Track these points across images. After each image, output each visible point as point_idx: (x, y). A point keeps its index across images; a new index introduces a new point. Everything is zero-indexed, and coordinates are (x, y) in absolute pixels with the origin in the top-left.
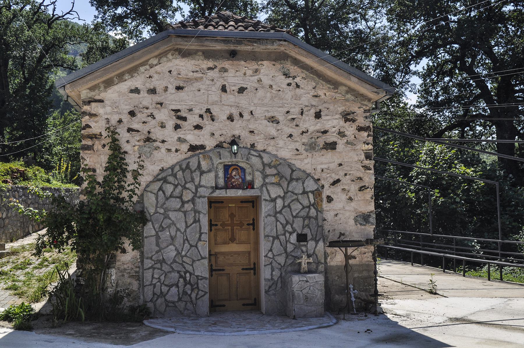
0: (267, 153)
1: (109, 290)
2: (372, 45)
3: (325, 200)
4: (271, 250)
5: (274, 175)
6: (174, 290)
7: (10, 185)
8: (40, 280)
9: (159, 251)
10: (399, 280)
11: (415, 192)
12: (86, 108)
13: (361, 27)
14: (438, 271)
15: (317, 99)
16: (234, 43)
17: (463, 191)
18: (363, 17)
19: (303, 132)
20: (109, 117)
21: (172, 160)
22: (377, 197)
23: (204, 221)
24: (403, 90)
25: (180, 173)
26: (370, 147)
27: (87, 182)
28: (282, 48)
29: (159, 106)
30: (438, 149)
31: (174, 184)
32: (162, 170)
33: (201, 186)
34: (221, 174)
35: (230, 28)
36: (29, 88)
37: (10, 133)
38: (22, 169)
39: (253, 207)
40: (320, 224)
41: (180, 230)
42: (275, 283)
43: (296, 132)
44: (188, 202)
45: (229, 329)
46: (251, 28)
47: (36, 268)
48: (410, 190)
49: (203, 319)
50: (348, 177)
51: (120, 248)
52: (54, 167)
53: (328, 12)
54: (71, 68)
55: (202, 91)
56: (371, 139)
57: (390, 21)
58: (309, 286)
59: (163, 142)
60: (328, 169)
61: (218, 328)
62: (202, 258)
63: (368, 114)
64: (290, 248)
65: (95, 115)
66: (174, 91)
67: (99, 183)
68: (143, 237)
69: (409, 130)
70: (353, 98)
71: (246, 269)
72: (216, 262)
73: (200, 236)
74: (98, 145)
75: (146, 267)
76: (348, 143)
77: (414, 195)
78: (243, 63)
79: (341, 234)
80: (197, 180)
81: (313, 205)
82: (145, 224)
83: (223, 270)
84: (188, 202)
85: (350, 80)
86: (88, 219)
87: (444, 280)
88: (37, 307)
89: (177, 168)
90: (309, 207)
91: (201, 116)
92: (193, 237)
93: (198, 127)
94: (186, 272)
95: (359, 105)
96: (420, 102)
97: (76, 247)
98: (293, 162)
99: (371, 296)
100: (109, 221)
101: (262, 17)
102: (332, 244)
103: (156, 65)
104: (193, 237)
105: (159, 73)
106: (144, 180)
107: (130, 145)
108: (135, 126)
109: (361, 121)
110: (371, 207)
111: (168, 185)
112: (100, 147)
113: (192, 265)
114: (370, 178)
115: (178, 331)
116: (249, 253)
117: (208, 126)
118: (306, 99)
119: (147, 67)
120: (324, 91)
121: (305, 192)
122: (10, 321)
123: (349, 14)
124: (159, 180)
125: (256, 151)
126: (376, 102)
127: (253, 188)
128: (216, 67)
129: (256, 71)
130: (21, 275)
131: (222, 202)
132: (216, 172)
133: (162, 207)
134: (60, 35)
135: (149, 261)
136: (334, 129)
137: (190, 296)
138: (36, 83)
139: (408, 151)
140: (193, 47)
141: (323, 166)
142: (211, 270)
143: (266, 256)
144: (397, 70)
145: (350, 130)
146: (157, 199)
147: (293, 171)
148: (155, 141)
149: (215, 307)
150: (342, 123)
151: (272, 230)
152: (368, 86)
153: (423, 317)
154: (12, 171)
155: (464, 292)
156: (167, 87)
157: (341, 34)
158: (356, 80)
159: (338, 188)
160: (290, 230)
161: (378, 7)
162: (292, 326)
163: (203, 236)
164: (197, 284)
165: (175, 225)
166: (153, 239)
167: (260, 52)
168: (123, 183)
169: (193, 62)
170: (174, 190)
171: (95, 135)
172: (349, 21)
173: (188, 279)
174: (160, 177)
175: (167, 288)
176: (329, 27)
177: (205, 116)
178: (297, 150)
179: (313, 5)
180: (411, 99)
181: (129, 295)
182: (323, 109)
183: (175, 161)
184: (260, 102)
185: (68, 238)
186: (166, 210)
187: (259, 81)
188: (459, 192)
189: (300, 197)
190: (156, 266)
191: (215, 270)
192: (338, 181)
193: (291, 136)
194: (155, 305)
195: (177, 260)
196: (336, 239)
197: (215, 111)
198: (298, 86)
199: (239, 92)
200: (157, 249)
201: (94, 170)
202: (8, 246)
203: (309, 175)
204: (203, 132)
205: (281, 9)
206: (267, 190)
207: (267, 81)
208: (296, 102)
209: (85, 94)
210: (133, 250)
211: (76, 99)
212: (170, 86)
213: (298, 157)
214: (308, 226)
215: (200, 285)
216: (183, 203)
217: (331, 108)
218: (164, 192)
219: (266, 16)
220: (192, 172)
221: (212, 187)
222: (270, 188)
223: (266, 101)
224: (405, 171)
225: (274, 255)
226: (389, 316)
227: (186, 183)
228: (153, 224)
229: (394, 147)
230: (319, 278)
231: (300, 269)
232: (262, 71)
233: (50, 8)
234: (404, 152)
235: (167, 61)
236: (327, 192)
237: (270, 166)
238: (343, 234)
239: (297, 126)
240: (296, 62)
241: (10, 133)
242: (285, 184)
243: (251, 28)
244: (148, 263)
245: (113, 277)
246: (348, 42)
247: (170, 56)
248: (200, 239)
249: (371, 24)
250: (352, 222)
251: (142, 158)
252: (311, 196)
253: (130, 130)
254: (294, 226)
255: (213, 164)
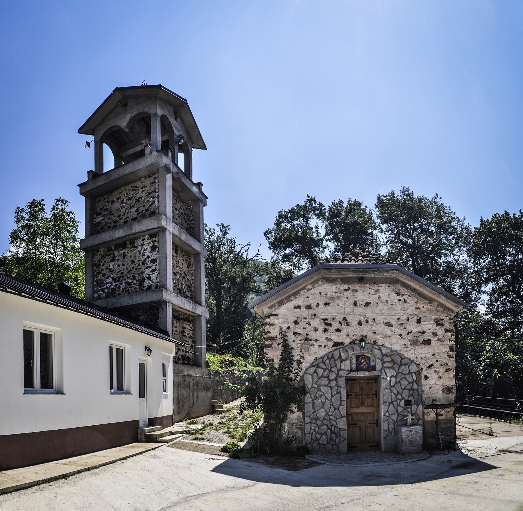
0: (385, 347)
1: (284, 436)
2: (457, 272)
3: (423, 378)
4: (388, 411)
5: (389, 362)
6: (324, 437)
7: (224, 370)
8: (243, 428)
9: (315, 412)
10: (471, 427)
11: (483, 370)
12: (267, 320)
13: (450, 260)
14: (495, 420)
15: (418, 310)
16: (362, 272)
17: (512, 370)
18: (452, 252)
19: (409, 333)
20: (281, 325)
21: (322, 352)
22: (457, 374)
23: (344, 392)
24: (477, 303)
25: (328, 361)
26: (453, 343)
27: (269, 368)
28: (395, 275)
29: (313, 317)
30: (497, 344)
31: (323, 369)
32: (316, 359)
33: (341, 370)
34: (354, 361)
35: (359, 261)
36: (233, 307)
37: (223, 336)
38: (230, 359)
39: (376, 383)
40: (420, 394)
41: (328, 399)
42: (391, 432)
43: (404, 333)
44: (333, 380)
45: (360, 462)
46: (373, 261)
47: (240, 420)
48: (480, 369)
49: (344, 456)
50: (438, 362)
51: (290, 410)
52: (250, 356)
53: (428, 248)
54: (258, 292)
55: (340, 306)
56: (453, 337)
57: (469, 256)
58: (411, 433)
59: (316, 340)
60: (425, 357)
61: (353, 461)
62: (342, 417)
63: (452, 321)
64: (400, 409)
65: (273, 325)
66: (323, 306)
67: (276, 369)
68: (304, 404)
69: (480, 330)
70: (442, 310)
71: (371, 423)
72: (352, 418)
73: (341, 402)
74: (275, 345)
75: (306, 422)
76: (438, 340)
77: (482, 372)
78: (368, 285)
79: (434, 400)
80: (339, 366)
81: (415, 382)
82: (305, 395)
83: (357, 424)
84: (333, 380)
85: (440, 297)
86: (270, 392)
87: (497, 426)
88: (242, 444)
89: (326, 358)
90: (412, 383)
91: (340, 323)
92: (336, 403)
93: (338, 330)
94: (332, 425)
95: (446, 315)
96: (487, 312)
97: (263, 409)
98: (402, 353)
99: (452, 439)
100: (282, 393)
101: (384, 251)
102: (428, 407)
103: (311, 289)
104: (336, 403)
105: (313, 295)
106: (305, 366)
107: (295, 343)
108: (298, 331)
109: (447, 326)
110: (453, 382)
111: (320, 369)
112: (276, 345)
113: (336, 421)
114: (452, 364)
115: (327, 463)
116: (374, 413)
117: (345, 330)
118: (411, 310)
119: (306, 291)
120: (423, 305)
121: (410, 373)
122: (227, 452)
123: (442, 250)
124: (314, 366)
125: (377, 345)
126: (457, 313)
127: (375, 370)
128: (350, 289)
129: (377, 291)
130: (232, 424)
131: (355, 380)
132: (351, 360)
133: (316, 384)
134: (251, 271)
135: (308, 418)
136: (429, 331)
137: (335, 441)
138: (237, 303)
139: (479, 344)
140: (334, 276)
141: (423, 356)
142: (349, 424)
143: (384, 415)
144: (473, 289)
145: (440, 331)
146: (313, 378)
147: (402, 359)
148: (311, 340)
149: (351, 448)
150: (435, 326)
151: (388, 398)
152: (452, 302)
153: (483, 451)
154: (225, 361)
155: (509, 433)
156: (318, 304)
157: (437, 263)
158: (444, 298)
159: (432, 370)
160: (400, 398)
161: (461, 246)
162: (401, 460)
163: (343, 402)
164: (340, 433)
165: (325, 395)
166: (311, 404)
167: (379, 278)
168: (291, 368)
169: (335, 286)
170: (324, 372)
171: (273, 337)
172: (442, 255)
173: (333, 430)
174: (314, 364)
175: (320, 436)
176: (429, 258)
177: (343, 323)
178: (405, 345)
179: (418, 243)
180: (482, 309)
181: (296, 440)
182: (422, 317)
183: (324, 353)
184: (380, 312)
185: (258, 403)
186: (319, 386)
187: (379, 298)
188: (509, 371)
189: (407, 376)
190: (313, 421)
191: (351, 424)
192: (432, 365)
193: (400, 335)
194: (312, 446)
195: (326, 418)
196: (430, 403)
197: (349, 318)
198: (405, 301)
199: (365, 306)
200: (313, 410)
201: (273, 361)
202: (225, 406)
203: (412, 361)
204: (341, 333)
205: (396, 245)
206: (385, 372)
207: (384, 298)
208: (404, 312)
209: (266, 311)
210: (298, 411)
211: (261, 315)
212: (320, 303)
213: (405, 349)
214: (412, 395)
215: (341, 434)
216: (330, 381)
217: (428, 316)
218: (317, 374)
219: (386, 250)
220: (335, 361)
221: (348, 370)
222: (387, 370)
223: (384, 312)
224: (477, 358)
225: (389, 415)
226: (463, 451)
227: (331, 368)
228: (310, 394)
229: (470, 341)
230: (418, 429)
231: (407, 423)
232: (381, 291)
233: (245, 254)
234: (476, 344)
235: (319, 286)
236: (424, 373)
237: (386, 355)
238: (435, 400)
239: (405, 328)
240: (404, 285)
241: (223, 336)
242: (397, 368)
243: (373, 261)
244: (307, 420)
245: (286, 428)
246: (441, 269)
247: (320, 283)
248: (340, 405)
249: (456, 257)
250: (441, 392)
251: (303, 352)
252: (414, 375)
253: (295, 333)
254: (403, 395)
255: (348, 355)
